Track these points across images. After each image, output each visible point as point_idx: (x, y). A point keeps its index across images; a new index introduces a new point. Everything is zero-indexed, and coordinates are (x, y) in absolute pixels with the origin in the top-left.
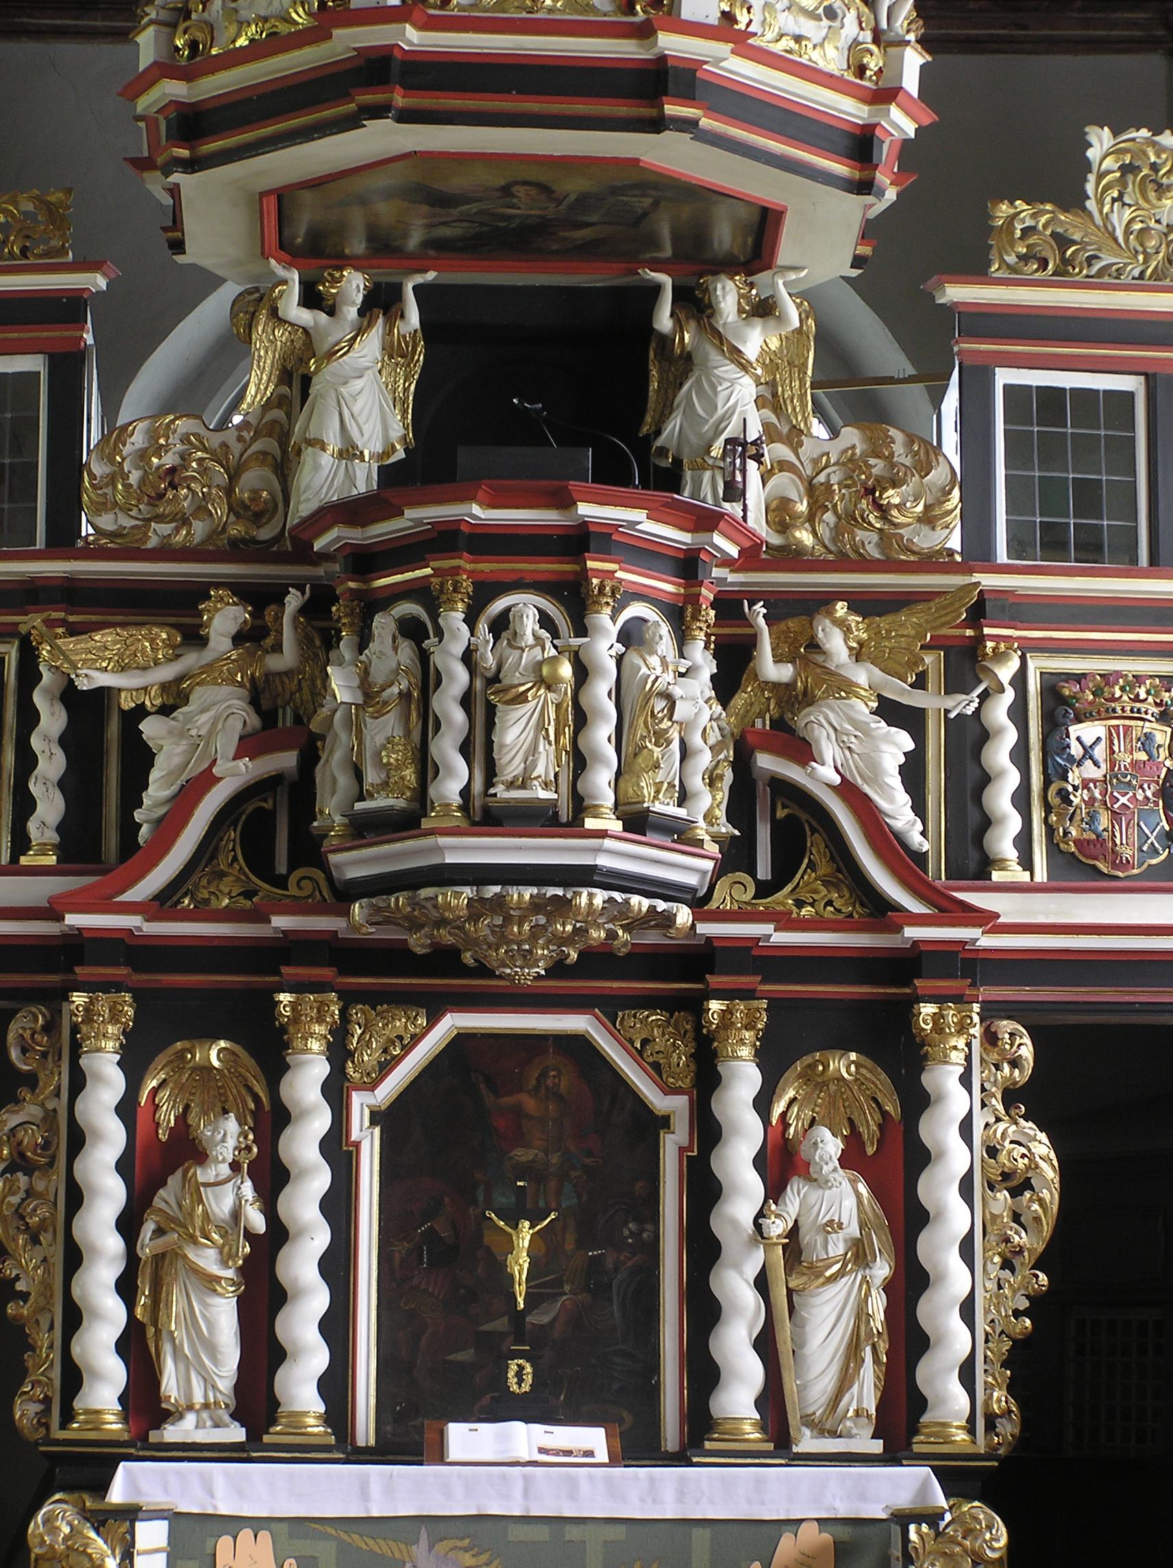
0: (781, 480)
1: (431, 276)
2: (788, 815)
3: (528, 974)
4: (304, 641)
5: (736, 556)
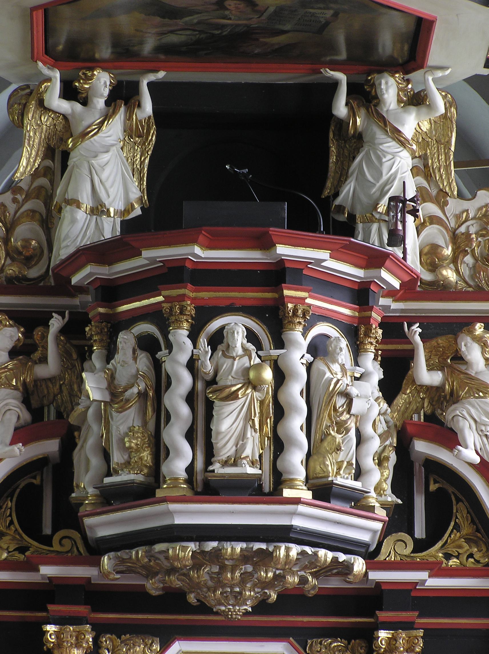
0: (432, 232)
1: (161, 74)
2: (439, 488)
3: (239, 611)
4: (64, 355)
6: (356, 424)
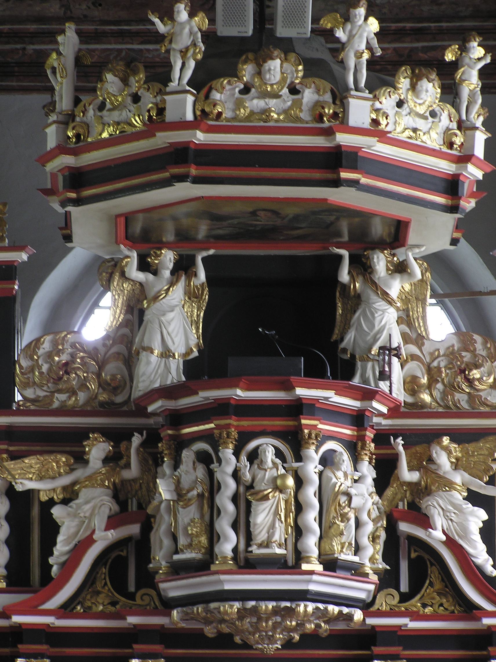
0: (413, 367)
3: (272, 648)
4: (143, 462)
5: (386, 413)
6: (355, 514)
